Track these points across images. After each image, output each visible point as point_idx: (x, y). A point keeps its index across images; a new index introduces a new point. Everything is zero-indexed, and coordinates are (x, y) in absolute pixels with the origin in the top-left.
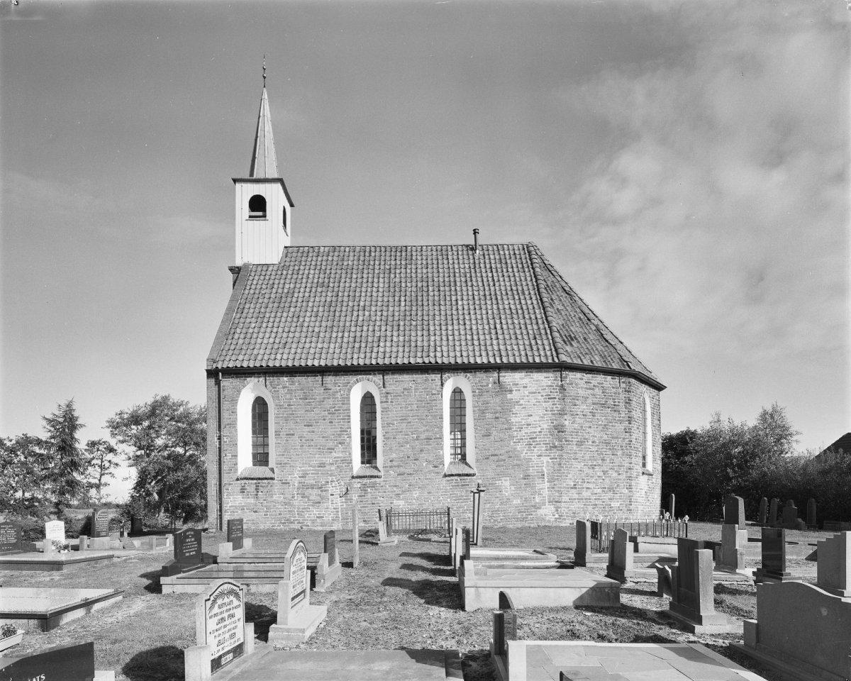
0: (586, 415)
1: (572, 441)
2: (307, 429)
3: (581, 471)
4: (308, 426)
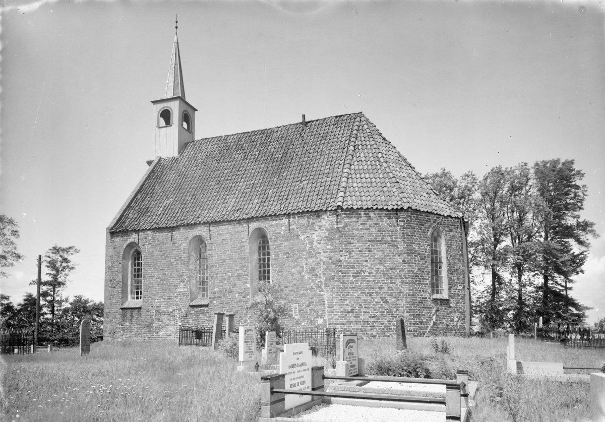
1: (349, 273)
3: (358, 298)
4: (162, 270)
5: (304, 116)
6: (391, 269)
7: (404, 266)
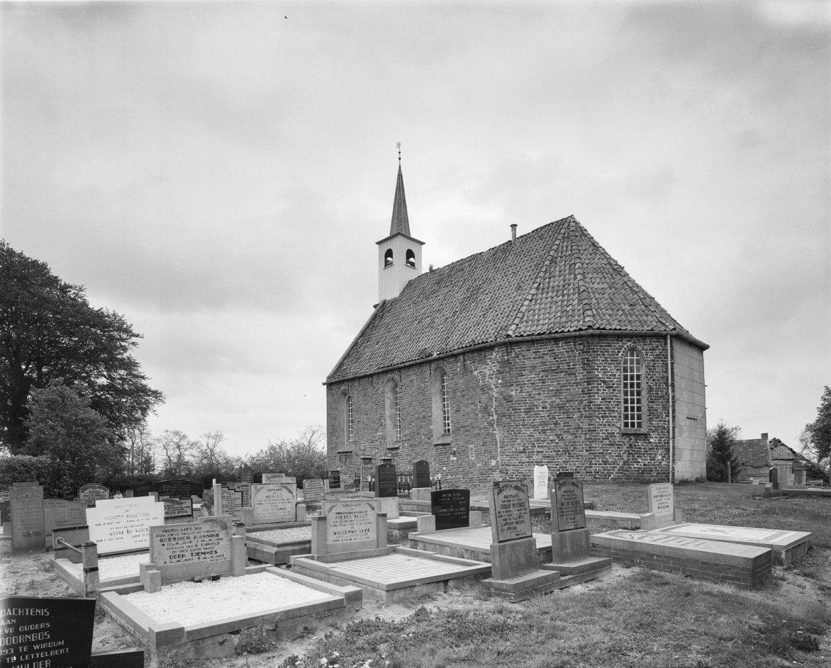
0: (534, 383)
1: (520, 409)
3: (531, 436)
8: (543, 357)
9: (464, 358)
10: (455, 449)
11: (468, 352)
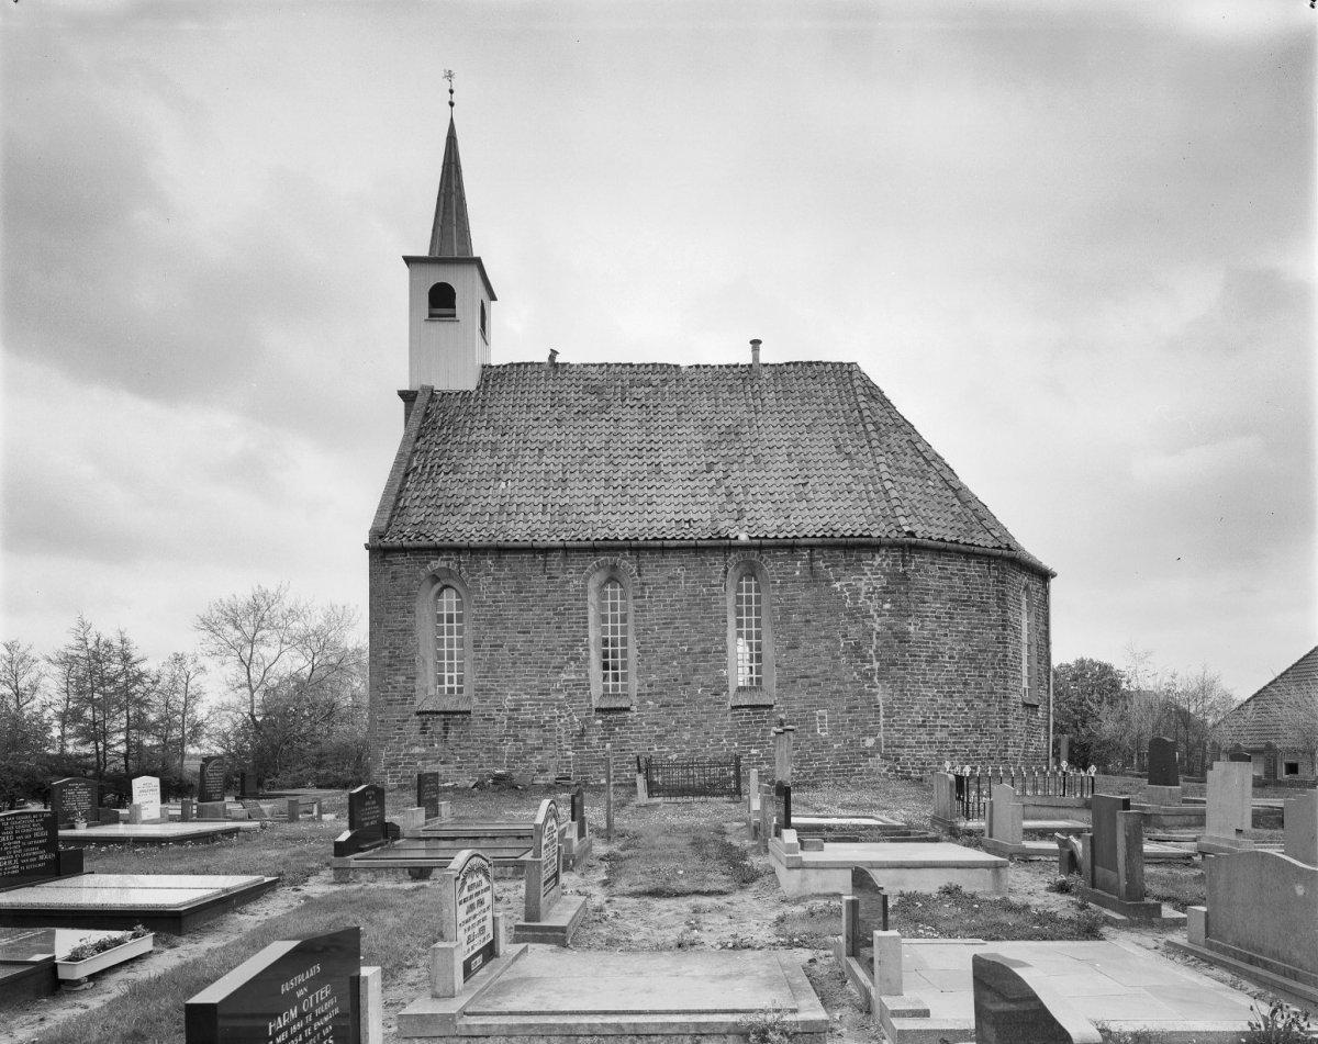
2: (522, 637)
4: (524, 633)
5: (554, 353)
6: (980, 651)
7: (998, 648)
8: (950, 578)
9: (810, 555)
10: (783, 716)
11: (819, 546)
